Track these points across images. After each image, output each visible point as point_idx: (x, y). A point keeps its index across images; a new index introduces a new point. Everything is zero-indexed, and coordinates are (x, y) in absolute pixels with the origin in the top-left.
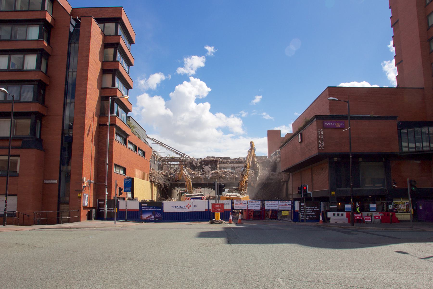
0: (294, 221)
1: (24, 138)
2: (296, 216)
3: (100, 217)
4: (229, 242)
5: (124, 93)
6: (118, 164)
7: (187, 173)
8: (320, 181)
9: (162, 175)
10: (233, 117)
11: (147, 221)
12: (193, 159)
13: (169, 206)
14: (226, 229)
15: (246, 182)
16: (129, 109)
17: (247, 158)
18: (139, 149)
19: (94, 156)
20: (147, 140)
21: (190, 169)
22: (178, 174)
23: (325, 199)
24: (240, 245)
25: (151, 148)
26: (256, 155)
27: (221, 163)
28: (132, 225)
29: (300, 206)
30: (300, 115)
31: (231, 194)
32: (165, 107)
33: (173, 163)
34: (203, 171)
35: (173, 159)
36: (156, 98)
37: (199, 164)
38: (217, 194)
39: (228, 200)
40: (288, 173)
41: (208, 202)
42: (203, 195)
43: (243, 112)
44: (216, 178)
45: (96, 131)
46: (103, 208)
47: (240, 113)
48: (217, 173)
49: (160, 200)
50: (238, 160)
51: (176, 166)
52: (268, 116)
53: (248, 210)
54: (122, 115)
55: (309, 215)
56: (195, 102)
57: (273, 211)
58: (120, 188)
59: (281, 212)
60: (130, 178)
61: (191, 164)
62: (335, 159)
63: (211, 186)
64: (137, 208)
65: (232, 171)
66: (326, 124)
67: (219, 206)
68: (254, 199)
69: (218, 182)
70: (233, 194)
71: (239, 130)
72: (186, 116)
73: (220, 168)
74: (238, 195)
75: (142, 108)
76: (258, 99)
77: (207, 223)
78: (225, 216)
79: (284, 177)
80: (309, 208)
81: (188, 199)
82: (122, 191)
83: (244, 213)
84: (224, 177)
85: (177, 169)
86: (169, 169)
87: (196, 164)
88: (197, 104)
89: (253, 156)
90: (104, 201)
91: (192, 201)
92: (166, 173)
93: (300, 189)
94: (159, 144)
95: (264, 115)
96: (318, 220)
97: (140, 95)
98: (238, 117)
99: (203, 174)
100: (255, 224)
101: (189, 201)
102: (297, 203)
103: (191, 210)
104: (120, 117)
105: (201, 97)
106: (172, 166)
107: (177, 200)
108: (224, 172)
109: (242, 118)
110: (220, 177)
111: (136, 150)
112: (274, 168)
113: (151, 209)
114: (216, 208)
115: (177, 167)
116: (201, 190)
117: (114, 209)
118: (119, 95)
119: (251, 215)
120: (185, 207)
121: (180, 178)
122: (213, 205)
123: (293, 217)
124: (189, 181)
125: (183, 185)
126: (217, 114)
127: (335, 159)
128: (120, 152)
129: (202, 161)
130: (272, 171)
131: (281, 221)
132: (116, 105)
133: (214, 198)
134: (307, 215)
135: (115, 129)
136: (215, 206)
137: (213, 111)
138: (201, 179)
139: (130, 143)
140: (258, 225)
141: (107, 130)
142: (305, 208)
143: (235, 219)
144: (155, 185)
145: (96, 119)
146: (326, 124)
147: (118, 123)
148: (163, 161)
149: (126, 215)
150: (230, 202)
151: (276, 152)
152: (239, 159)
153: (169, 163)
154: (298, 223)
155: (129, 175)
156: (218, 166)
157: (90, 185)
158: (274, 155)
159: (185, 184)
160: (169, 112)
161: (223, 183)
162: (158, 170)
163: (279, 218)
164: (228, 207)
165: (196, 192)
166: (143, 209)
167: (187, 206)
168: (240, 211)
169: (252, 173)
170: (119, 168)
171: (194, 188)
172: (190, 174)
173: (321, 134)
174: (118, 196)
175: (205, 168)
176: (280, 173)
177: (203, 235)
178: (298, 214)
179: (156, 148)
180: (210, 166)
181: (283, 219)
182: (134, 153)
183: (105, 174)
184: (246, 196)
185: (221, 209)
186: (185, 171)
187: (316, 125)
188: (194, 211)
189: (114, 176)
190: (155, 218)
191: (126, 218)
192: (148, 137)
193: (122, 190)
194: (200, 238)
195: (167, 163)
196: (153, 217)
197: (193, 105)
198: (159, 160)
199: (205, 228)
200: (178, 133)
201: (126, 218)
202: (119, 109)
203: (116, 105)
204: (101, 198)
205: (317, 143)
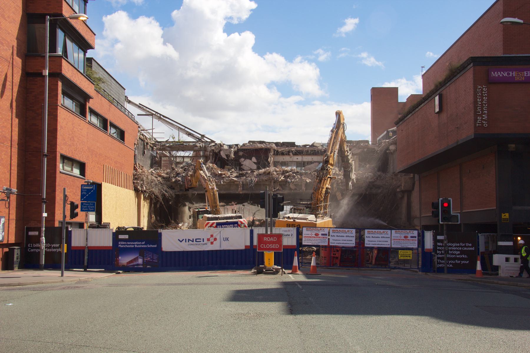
0: (423, 271)
2: (427, 261)
3: (30, 262)
4: (292, 310)
5: (77, 10)
6: (69, 155)
8: (478, 193)
9: (159, 178)
10: (301, 62)
11: (127, 269)
12: (221, 145)
13: (172, 240)
14: (285, 284)
15: (327, 192)
16: (90, 42)
17: (329, 144)
18: (113, 125)
19: (16, 137)
20: (128, 106)
21: (215, 166)
22: (191, 175)
23: (489, 228)
24: (315, 316)
25: (137, 123)
26: (348, 139)
27: (277, 153)
28: (98, 278)
29: (435, 241)
30: (437, 56)
31: (296, 215)
32: (162, 40)
33: (181, 153)
35: (181, 146)
36: (143, 21)
37: (232, 156)
38: (268, 215)
39: (291, 228)
40: (412, 175)
41: (252, 232)
42: (240, 217)
43: (320, 51)
44: (267, 183)
45: (20, 86)
46: (37, 245)
47: (315, 53)
48: (269, 173)
49: (155, 227)
50: (312, 149)
51: (186, 160)
52: (372, 59)
53: (330, 248)
54: (76, 55)
55: (454, 259)
56: (224, 31)
57: (379, 249)
58: (72, 204)
59: (398, 252)
60: (93, 184)
61: (217, 156)
62: (512, 146)
63: (255, 198)
64: (108, 242)
65: (299, 169)
66: (495, 74)
67: (271, 239)
68: (343, 225)
69: (270, 191)
70: (301, 216)
71: (311, 87)
72: (205, 59)
73: (276, 164)
74: (311, 218)
75: (117, 41)
76: (351, 24)
77: (249, 272)
78: (285, 259)
79: (404, 182)
80: (454, 245)
81: (211, 226)
82: (78, 210)
83: (322, 253)
84: (282, 181)
85: (189, 165)
87: (227, 155)
88: (229, 35)
89: (342, 139)
90: (39, 230)
91: (219, 229)
92: (167, 174)
93: (435, 206)
94: (152, 115)
95: (363, 58)
96: (473, 270)
97: (110, 13)
98: (310, 61)
100: (343, 275)
101: (212, 228)
102: (429, 236)
103: (215, 247)
104: (70, 59)
105: (235, 22)
106: (178, 160)
107: (190, 228)
108: (284, 172)
109: (320, 65)
110: (276, 181)
111: (105, 128)
112: (384, 164)
113: (136, 244)
114: (266, 243)
115: (190, 162)
117: (60, 247)
118: (66, 12)
119: (337, 258)
120: (206, 241)
121: (195, 184)
122: (260, 236)
123: (420, 262)
124: (213, 189)
125: (201, 198)
126: (268, 56)
127: (512, 146)
128: (72, 132)
129: (239, 150)
130: (379, 170)
131: (396, 270)
132: (60, 35)
133: (262, 224)
134: (449, 259)
135: (60, 84)
136: (265, 239)
137: (260, 49)
138: (237, 185)
139: (93, 112)
140: (346, 277)
141: (44, 86)
142: (446, 246)
143: (304, 265)
144: (144, 198)
145: (18, 62)
146: (495, 74)
147: (67, 71)
148: (160, 150)
149: (86, 258)
150: (294, 231)
151: (388, 132)
152: (313, 145)
153: (174, 153)
154: (431, 275)
155: (91, 176)
156: (271, 159)
157: (9, 198)
158: (383, 138)
160: (170, 51)
161: (281, 194)
162: (151, 167)
163: (392, 265)
164: (290, 241)
165: (227, 213)
166: (121, 245)
167: (208, 240)
168: (315, 248)
169: (338, 175)
170: (70, 163)
171: (222, 204)
172: (215, 175)
173: (482, 96)
174: (68, 219)
176: (396, 175)
177: (239, 296)
178: (432, 256)
179: (146, 122)
180: (254, 159)
181: (401, 266)
182: (101, 134)
183: (41, 175)
184: (327, 219)
185: (277, 246)
186: (205, 173)
187: (472, 76)
188: (222, 249)
189: (59, 178)
190: (145, 263)
191: (86, 264)
192: (129, 102)
193: (77, 207)
194: (233, 303)
195: (168, 154)
196: (140, 261)
197: (219, 37)
198: (153, 148)
199: (242, 284)
200: (190, 93)
201: (86, 264)
202: (69, 42)
203: (60, 35)
204: (32, 224)
205: (472, 114)
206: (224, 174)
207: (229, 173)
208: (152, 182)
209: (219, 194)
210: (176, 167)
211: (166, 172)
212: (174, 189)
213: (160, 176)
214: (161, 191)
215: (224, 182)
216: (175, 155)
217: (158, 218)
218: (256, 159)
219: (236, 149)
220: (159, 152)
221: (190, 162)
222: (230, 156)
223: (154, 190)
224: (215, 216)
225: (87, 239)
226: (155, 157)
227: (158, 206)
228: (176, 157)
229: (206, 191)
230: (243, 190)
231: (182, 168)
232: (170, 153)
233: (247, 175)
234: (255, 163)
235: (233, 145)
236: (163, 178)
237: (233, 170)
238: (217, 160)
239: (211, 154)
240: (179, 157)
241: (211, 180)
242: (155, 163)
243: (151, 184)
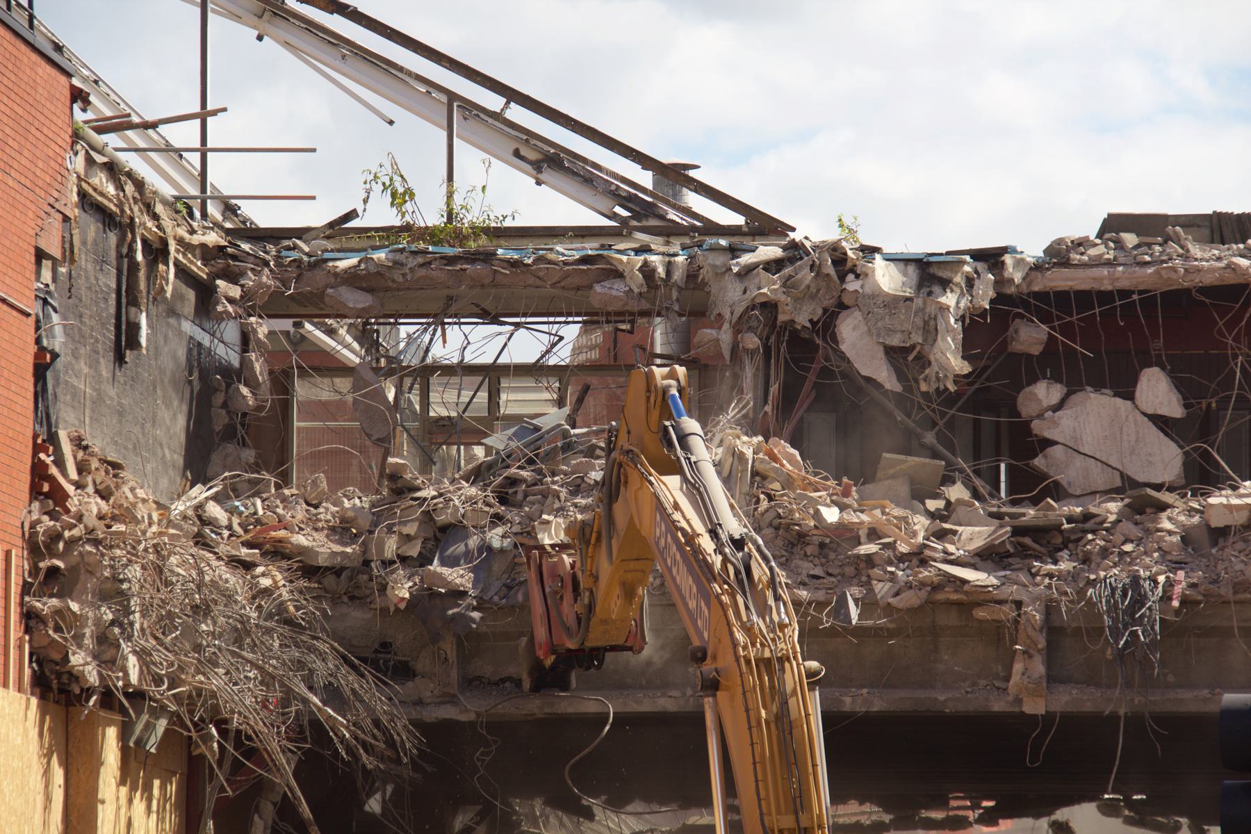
1: (357, 288)
7: (733, 526)
9: (270, 576)
12: (842, 263)
33: (474, 342)
35: (471, 271)
37: (951, 358)
61: (792, 335)
85: (542, 449)
86: (402, 458)
87: (894, 354)
92: (343, 529)
106: (445, 402)
115: (553, 417)
124: (771, 666)
129: (1009, 306)
138: (999, 637)
144: (131, 757)
148: (273, 307)
162: (197, 466)
180: (1157, 391)
195: (349, 351)
198: (205, 294)
206: (874, 534)
215: (868, 604)
219: (984, 294)
222: (923, 361)
230: (1054, 678)
235: (952, 260)
242: (229, 434)
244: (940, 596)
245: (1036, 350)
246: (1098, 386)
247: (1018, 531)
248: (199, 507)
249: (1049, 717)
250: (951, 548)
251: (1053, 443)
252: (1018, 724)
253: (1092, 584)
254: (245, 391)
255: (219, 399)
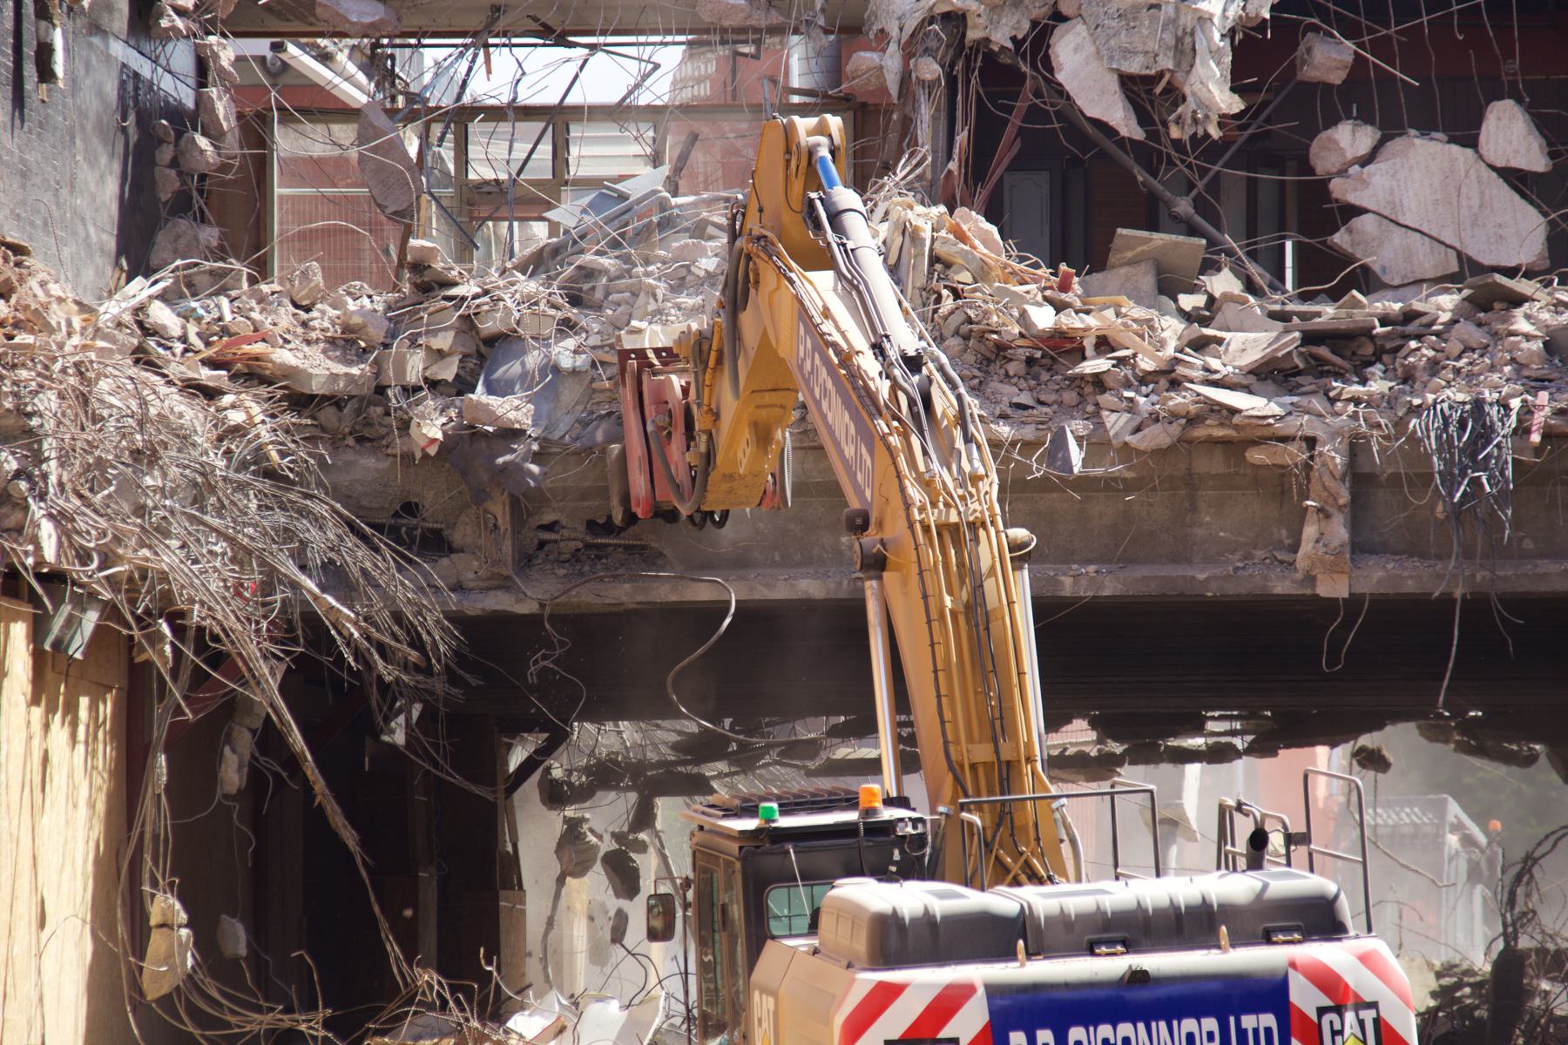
7: (906, 337)
9: (244, 407)
34: (1330, 272)
37: (1213, 90)
42: (1318, 919)
51: (594, 154)
85: (633, 225)
86: (432, 240)
87: (1137, 89)
92: (346, 342)
99: (1342, 352)
106: (491, 156)
115: (645, 180)
116: (1264, 784)
138: (1285, 490)
149: (377, 909)
159: (848, 622)
162: (136, 250)
171: (1079, 735)
172: (986, 356)
175: (1373, 188)
180: (1510, 133)
195: (349, 82)
206: (1104, 345)
207: (1172, 329)
208: (145, 457)
209: (1043, 609)
210: (466, 245)
211: (324, 318)
212: (436, 544)
213: (253, 375)
214: (271, 580)
215: (1096, 445)
216: (441, 97)
217: (236, 938)
218: (1543, 124)
220: (227, 51)
221: (645, 180)
222: (1175, 96)
223: (169, 558)
224: (972, 900)
225: (35, 865)
226: (185, 120)
227: (232, 774)
228: (462, 116)
229: (876, 564)
230: (1361, 547)
231: (538, 263)
232: (377, 66)
233: (1420, 353)
234: (1516, 179)
236: (299, 400)
237: (1223, 283)
238: (1007, 148)
239: (930, 69)
240: (495, 114)
241: (943, 402)
242: (181, 204)
243: (129, 487)
244: (1199, 432)
245: (1337, 78)
246: (1426, 128)
247: (1310, 338)
248: (140, 309)
249: (1354, 601)
250: (1215, 363)
251: (1360, 211)
252: (1308, 614)
253: (1415, 411)
254: (203, 142)
255: (166, 154)
